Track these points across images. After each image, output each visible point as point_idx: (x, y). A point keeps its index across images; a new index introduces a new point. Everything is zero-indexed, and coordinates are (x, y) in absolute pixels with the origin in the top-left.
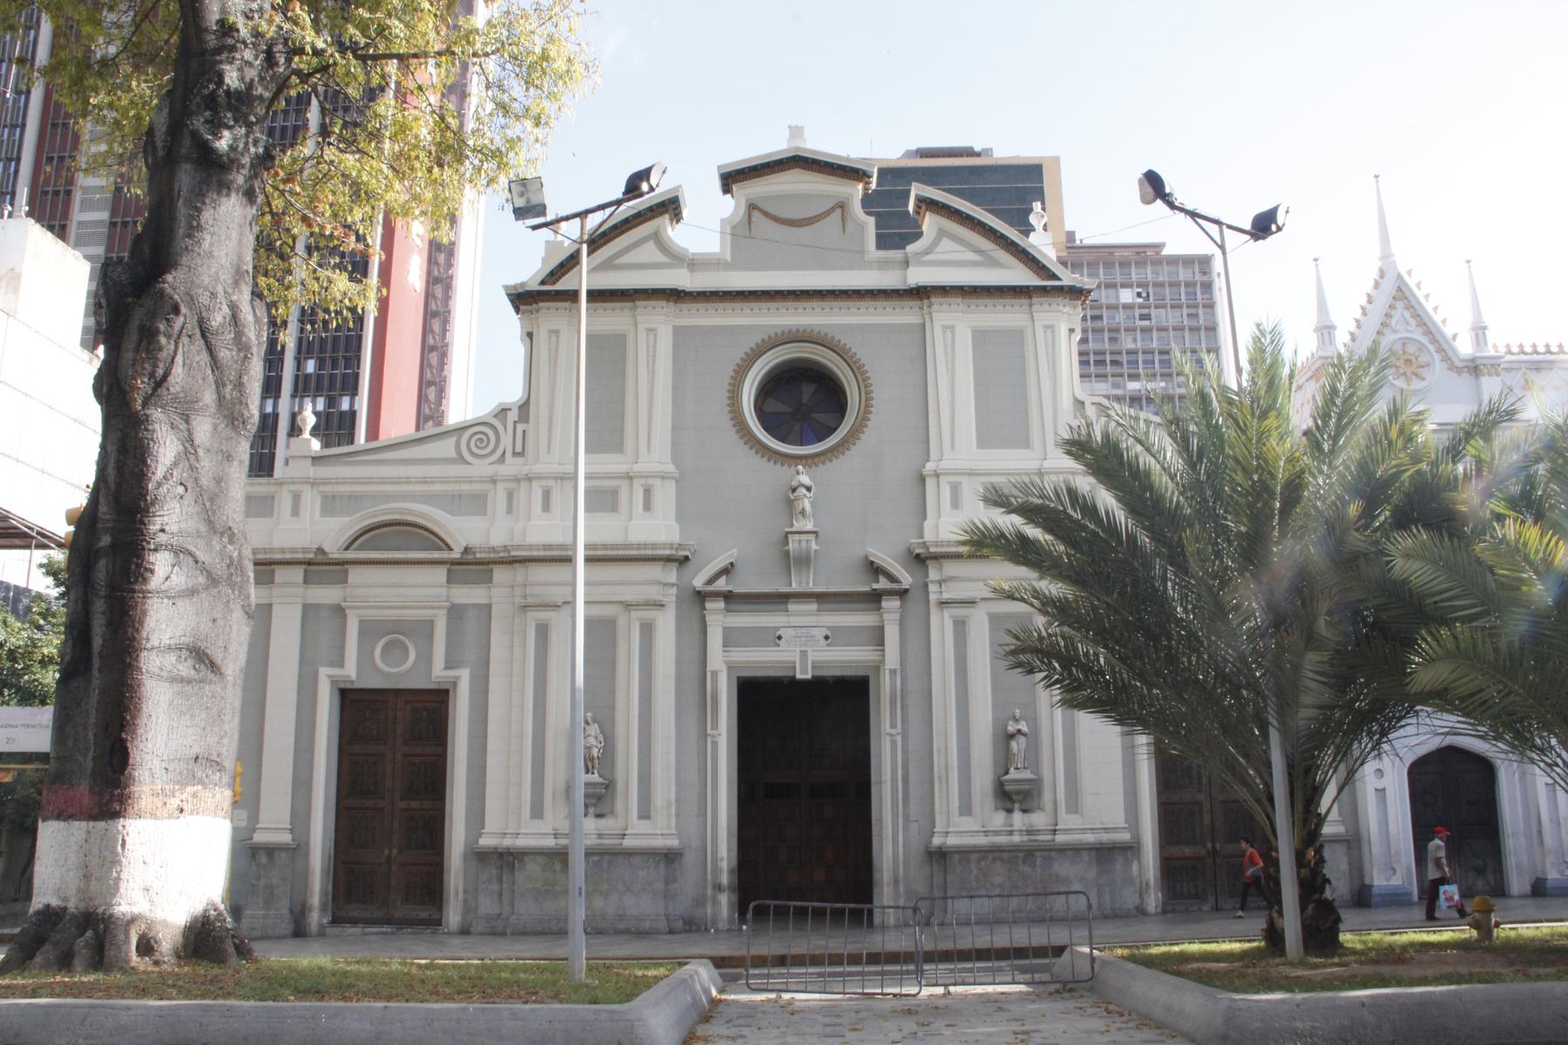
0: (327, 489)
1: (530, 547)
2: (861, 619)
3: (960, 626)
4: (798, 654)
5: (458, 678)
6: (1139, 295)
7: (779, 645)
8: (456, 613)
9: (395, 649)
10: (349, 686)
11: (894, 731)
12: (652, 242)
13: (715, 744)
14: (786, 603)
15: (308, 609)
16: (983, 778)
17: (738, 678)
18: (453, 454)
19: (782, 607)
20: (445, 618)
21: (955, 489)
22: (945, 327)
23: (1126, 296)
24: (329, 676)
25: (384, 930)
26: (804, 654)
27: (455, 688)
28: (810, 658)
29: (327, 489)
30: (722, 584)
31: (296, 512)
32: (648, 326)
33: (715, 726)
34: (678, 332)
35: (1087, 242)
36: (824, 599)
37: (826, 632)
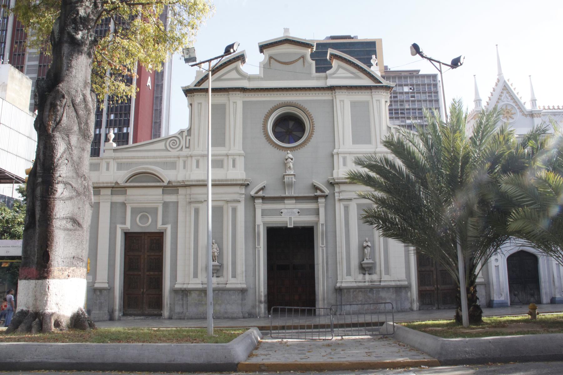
0: (119, 161)
2: (311, 206)
3: (346, 208)
6: (411, 89)
7: (281, 215)
8: (166, 205)
9: (144, 218)
10: (127, 231)
11: (323, 246)
12: (234, 71)
13: (259, 251)
14: (284, 200)
15: (112, 204)
17: (267, 227)
18: (164, 148)
21: (344, 159)
22: (340, 101)
23: (406, 89)
24: (120, 228)
25: (142, 318)
26: (290, 218)
27: (166, 232)
28: (293, 220)
29: (119, 161)
30: (261, 194)
31: (108, 169)
32: (377, 99)
33: (259, 244)
35: (392, 70)
36: (297, 199)
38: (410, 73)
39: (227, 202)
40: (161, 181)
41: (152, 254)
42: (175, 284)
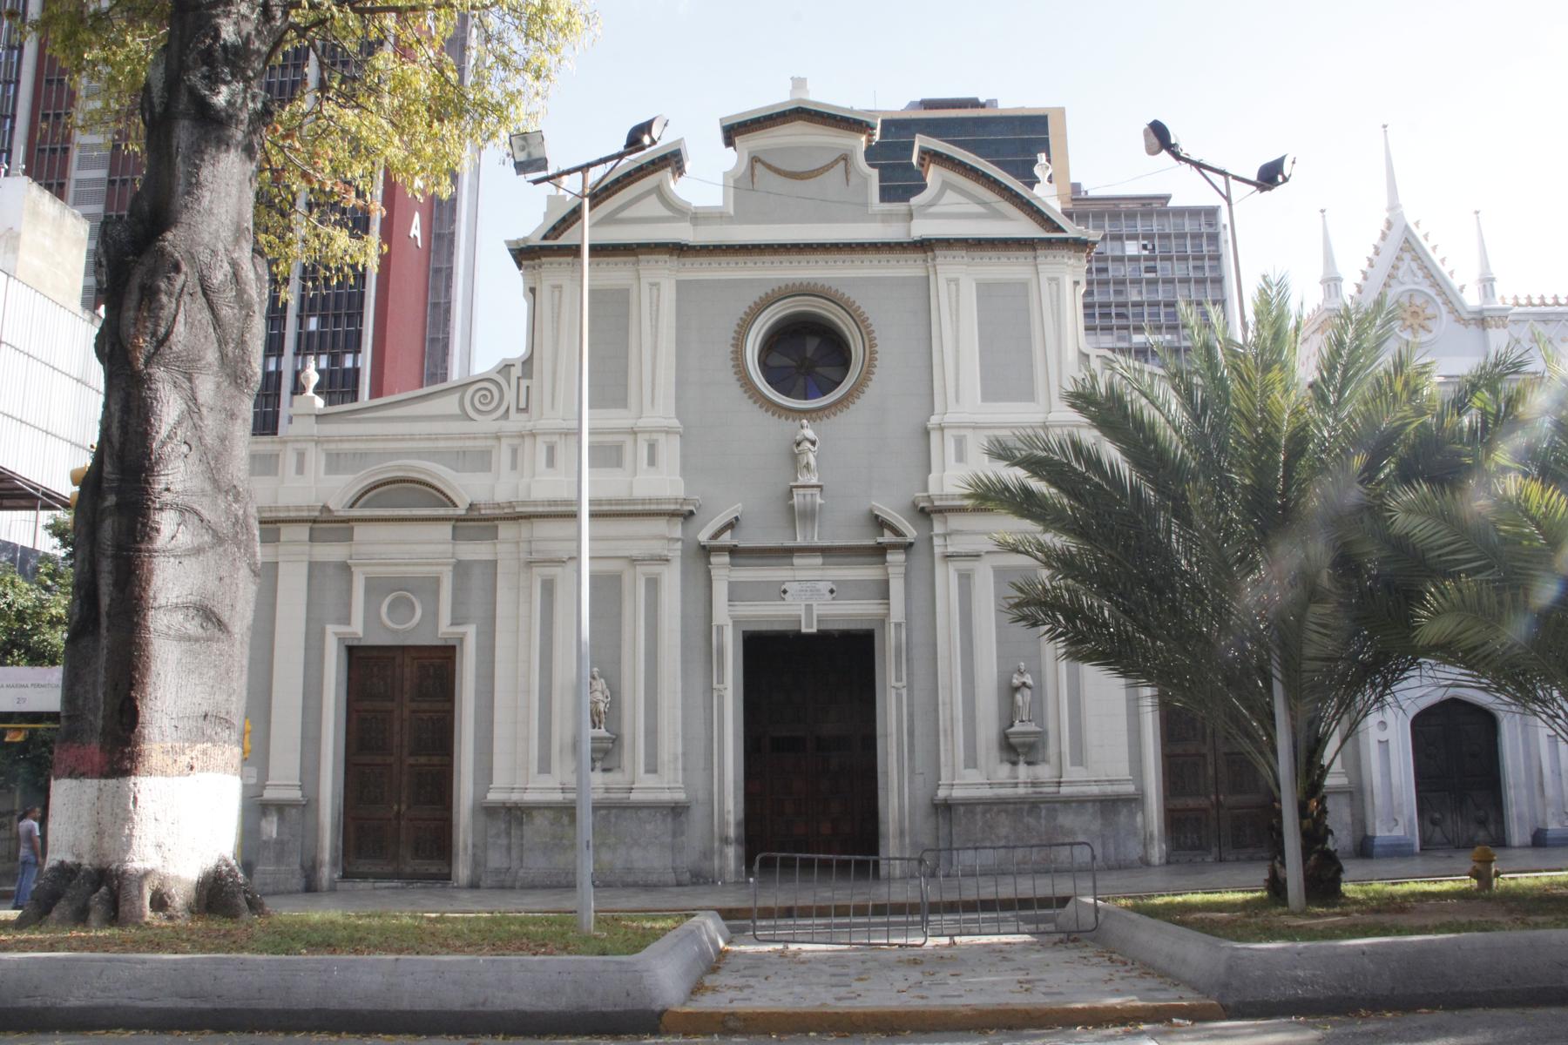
0: (332, 446)
1: (535, 503)
3: (965, 579)
4: (803, 607)
5: (464, 634)
6: (1145, 247)
7: (784, 599)
8: (462, 569)
9: (402, 606)
10: (355, 643)
13: (721, 698)
16: (988, 731)
17: (744, 632)
19: (788, 561)
20: (450, 574)
22: (949, 281)
23: (1132, 248)
24: (336, 634)
26: (809, 608)
30: (726, 539)
31: (300, 469)
32: (1050, 275)
33: (721, 680)
34: (681, 285)
35: (1091, 194)
37: (830, 586)
38: (1144, 205)
39: (633, 561)
40: (450, 504)
41: (425, 706)
42: (488, 790)
